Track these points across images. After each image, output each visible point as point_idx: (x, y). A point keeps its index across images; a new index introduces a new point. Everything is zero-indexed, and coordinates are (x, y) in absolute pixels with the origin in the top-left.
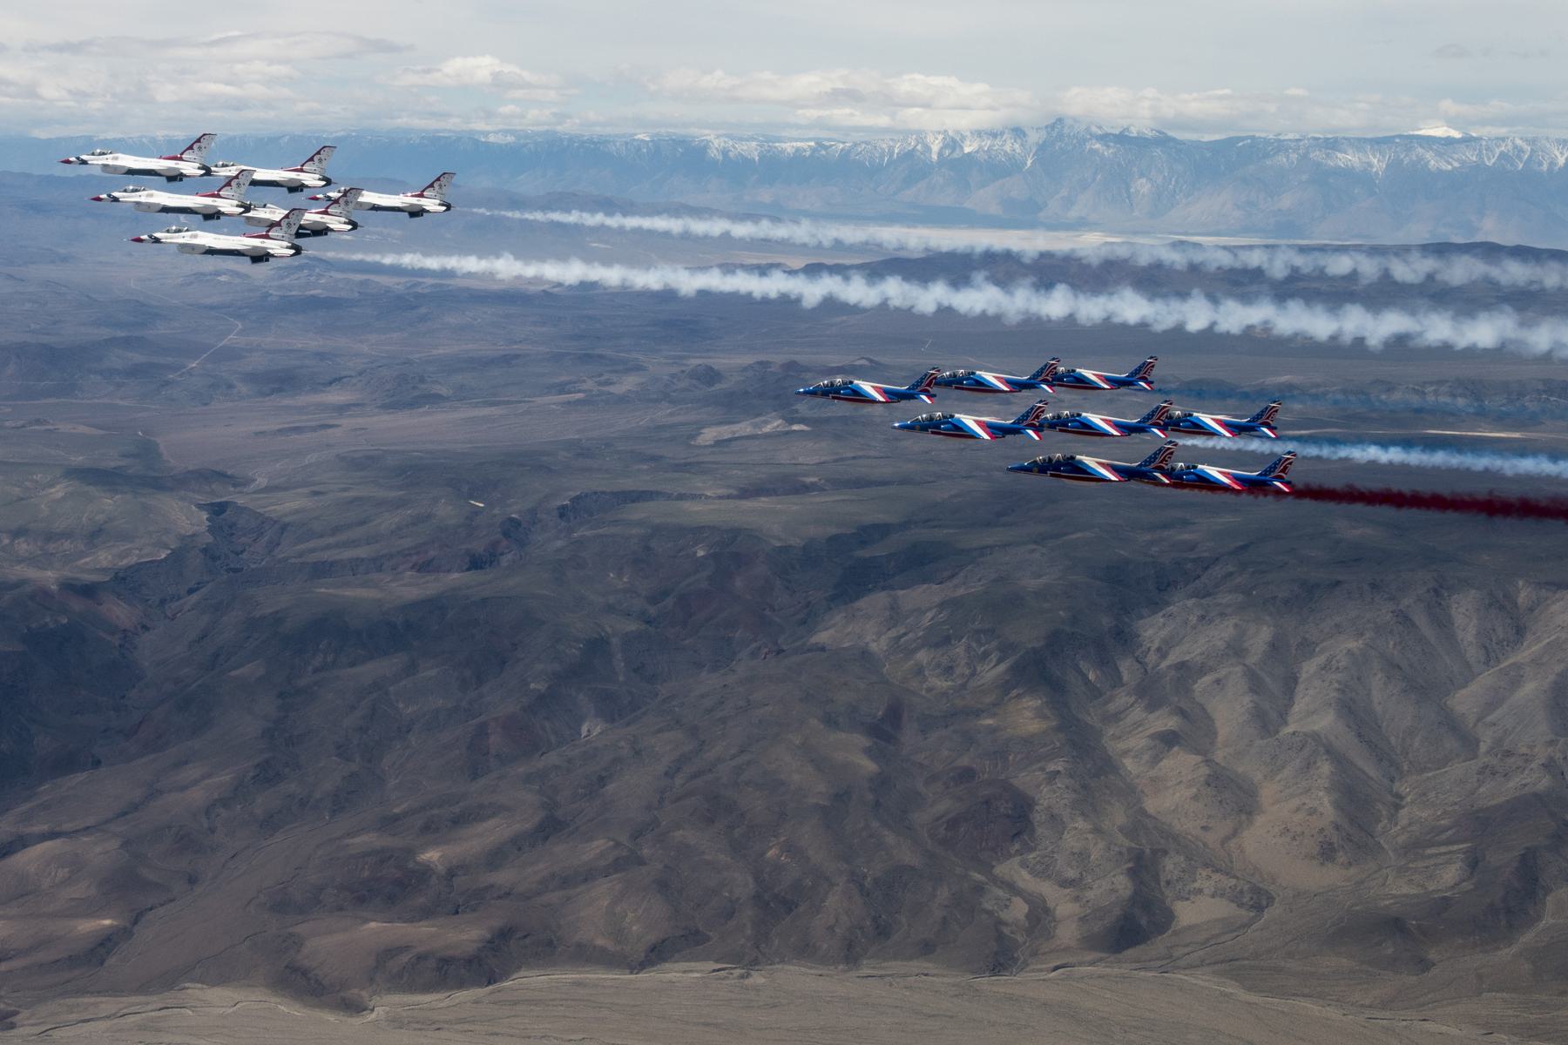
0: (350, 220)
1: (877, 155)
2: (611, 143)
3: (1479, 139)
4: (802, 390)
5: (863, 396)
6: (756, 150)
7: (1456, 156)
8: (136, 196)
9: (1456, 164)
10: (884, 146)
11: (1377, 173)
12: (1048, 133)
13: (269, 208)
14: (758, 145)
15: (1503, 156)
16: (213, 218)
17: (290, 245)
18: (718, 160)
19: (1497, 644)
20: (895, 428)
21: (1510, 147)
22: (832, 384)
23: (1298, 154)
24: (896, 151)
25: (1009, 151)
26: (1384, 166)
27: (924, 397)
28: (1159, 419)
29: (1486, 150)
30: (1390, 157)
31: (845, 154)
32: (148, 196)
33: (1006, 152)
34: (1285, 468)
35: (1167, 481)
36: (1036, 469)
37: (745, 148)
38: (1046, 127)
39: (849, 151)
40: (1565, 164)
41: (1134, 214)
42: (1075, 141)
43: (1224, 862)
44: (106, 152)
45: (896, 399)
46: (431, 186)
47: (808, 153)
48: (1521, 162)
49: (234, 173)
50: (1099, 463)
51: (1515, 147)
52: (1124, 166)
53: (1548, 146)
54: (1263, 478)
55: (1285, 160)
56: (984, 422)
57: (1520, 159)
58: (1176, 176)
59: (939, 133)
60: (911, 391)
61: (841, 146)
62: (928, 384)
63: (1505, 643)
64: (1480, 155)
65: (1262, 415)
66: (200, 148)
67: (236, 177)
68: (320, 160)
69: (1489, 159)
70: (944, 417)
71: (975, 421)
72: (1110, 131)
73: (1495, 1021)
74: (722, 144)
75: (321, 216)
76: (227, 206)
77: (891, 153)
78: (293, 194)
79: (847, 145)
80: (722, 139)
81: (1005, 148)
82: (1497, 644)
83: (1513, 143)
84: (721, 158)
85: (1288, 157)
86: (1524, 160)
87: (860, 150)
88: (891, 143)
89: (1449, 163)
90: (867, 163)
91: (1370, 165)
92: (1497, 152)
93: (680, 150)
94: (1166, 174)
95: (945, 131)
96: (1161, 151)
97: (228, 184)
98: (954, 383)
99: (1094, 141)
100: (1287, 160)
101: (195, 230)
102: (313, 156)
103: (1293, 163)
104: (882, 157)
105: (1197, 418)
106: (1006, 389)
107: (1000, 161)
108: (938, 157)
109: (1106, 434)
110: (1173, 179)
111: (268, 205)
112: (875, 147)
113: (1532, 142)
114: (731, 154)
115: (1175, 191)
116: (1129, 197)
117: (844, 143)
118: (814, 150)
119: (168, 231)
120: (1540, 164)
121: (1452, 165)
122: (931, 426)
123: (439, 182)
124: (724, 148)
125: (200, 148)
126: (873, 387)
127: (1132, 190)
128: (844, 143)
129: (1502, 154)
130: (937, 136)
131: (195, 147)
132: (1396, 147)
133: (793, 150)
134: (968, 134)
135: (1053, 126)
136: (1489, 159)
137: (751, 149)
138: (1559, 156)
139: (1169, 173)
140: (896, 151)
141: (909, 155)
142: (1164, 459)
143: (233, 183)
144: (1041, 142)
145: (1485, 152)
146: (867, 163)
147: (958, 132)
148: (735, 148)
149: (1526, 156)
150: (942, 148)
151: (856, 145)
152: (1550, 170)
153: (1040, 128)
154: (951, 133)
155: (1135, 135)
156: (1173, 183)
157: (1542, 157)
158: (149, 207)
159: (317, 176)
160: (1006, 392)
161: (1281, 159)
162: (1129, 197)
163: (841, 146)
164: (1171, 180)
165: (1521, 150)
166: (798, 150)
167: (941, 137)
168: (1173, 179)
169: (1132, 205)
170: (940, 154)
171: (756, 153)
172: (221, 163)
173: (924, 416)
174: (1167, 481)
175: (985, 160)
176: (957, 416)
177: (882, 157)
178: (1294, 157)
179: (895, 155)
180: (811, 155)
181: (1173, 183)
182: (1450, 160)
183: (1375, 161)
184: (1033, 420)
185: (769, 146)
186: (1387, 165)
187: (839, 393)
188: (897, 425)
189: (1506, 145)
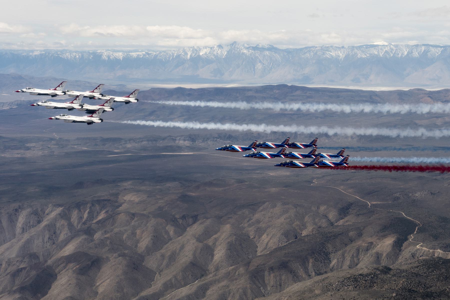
1: (168, 57)
2: (65, 54)
3: (377, 46)
4: (217, 149)
6: (122, 55)
7: (368, 52)
8: (46, 104)
9: (368, 55)
10: (171, 53)
11: (341, 59)
12: (231, 47)
14: (122, 54)
15: (386, 52)
16: (71, 110)
17: (99, 119)
18: (106, 60)
19: (29, 227)
20: (244, 157)
21: (389, 48)
22: (226, 147)
23: (314, 53)
24: (175, 55)
25: (216, 54)
26: (344, 57)
27: (253, 149)
28: (314, 153)
29: (381, 50)
30: (346, 53)
31: (156, 56)
32: (50, 104)
33: (214, 54)
35: (318, 166)
36: (282, 165)
37: (117, 55)
38: (231, 45)
39: (157, 56)
41: (255, 77)
43: (260, 244)
45: (245, 150)
46: (59, 86)
47: (142, 56)
48: (392, 53)
51: (391, 48)
52: (254, 59)
53: (402, 48)
55: (309, 55)
56: (269, 154)
57: (391, 52)
59: (191, 47)
60: (309, 155)
61: (155, 53)
62: (254, 146)
63: (32, 227)
64: (378, 52)
65: (285, 142)
69: (381, 53)
70: (258, 153)
71: (266, 153)
72: (252, 46)
74: (108, 54)
75: (71, 104)
76: (76, 106)
77: (173, 55)
79: (157, 53)
80: (108, 52)
81: (214, 53)
82: (29, 227)
83: (390, 47)
84: (107, 59)
85: (310, 54)
86: (393, 53)
87: (161, 55)
88: (173, 52)
89: (366, 55)
90: (164, 60)
91: (339, 56)
92: (384, 50)
93: (92, 56)
95: (194, 47)
96: (268, 53)
98: (260, 146)
99: (244, 50)
100: (310, 55)
103: (311, 56)
104: (169, 58)
105: (267, 144)
106: (274, 147)
107: (212, 58)
108: (190, 57)
109: (238, 151)
110: (272, 63)
112: (167, 53)
113: (396, 46)
114: (111, 58)
115: (272, 68)
116: (254, 71)
117: (156, 52)
119: (60, 116)
120: (398, 54)
121: (366, 56)
122: (254, 156)
123: (61, 85)
124: (109, 55)
128: (156, 52)
129: (386, 50)
130: (190, 49)
133: (137, 55)
134: (202, 48)
135: (233, 44)
136: (381, 53)
137: (120, 55)
138: (405, 50)
140: (175, 55)
141: (178, 56)
142: (317, 161)
144: (228, 50)
145: (380, 50)
146: (164, 60)
149: (394, 52)
151: (160, 53)
154: (195, 48)
155: (261, 47)
156: (271, 64)
157: (399, 52)
158: (50, 107)
160: (275, 148)
162: (254, 71)
163: (155, 53)
164: (270, 63)
165: (393, 50)
166: (138, 55)
167: (191, 49)
168: (272, 63)
169: (255, 73)
171: (121, 57)
172: (28, 88)
173: (252, 153)
174: (318, 166)
176: (261, 152)
177: (169, 58)
179: (175, 57)
180: (142, 58)
181: (271, 64)
182: (366, 54)
183: (341, 55)
184: (283, 152)
185: (127, 54)
187: (228, 149)
188: (244, 156)
189: (388, 48)
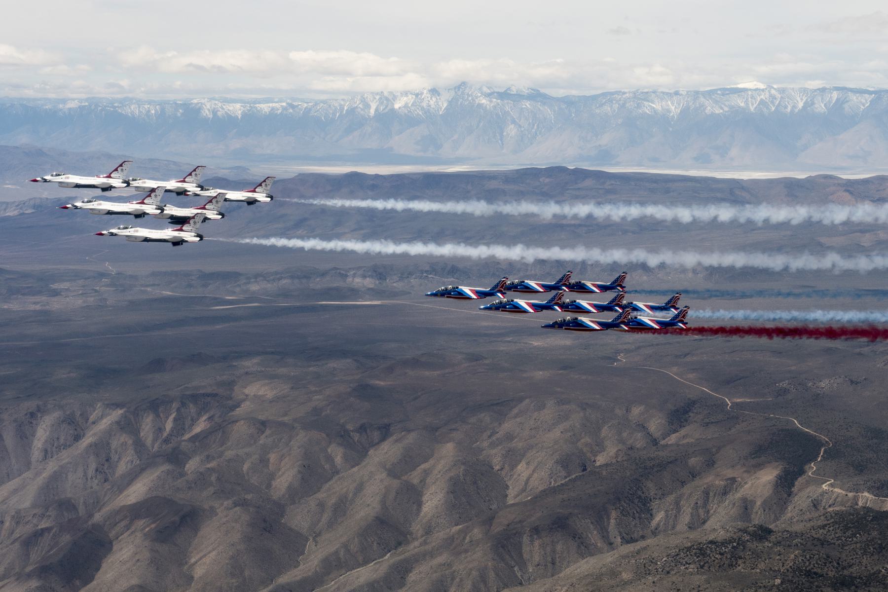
0: (220, 212)
3: (745, 90)
5: (583, 309)
7: (727, 103)
8: (90, 205)
9: (726, 109)
10: (337, 105)
11: (673, 116)
12: (456, 93)
13: (167, 207)
15: (762, 102)
16: (141, 217)
17: (196, 234)
18: (209, 118)
20: (481, 309)
21: (767, 95)
22: (446, 289)
23: (619, 104)
24: (346, 109)
25: (425, 107)
26: (679, 112)
27: (499, 294)
29: (751, 98)
30: (683, 105)
31: (308, 111)
32: (98, 204)
33: (423, 107)
34: (684, 315)
35: (627, 329)
36: (557, 326)
37: (231, 108)
38: (455, 88)
39: (310, 110)
40: (803, 107)
41: (503, 151)
42: (470, 98)
44: (60, 173)
45: (483, 296)
47: (279, 111)
48: (774, 106)
49: (215, 195)
50: (591, 321)
51: (771, 96)
52: (501, 116)
54: (549, 304)
55: (609, 109)
56: (531, 303)
57: (772, 102)
58: (538, 123)
59: (377, 94)
60: (610, 305)
61: (306, 105)
64: (746, 102)
66: (122, 170)
67: (216, 197)
68: (196, 175)
70: (508, 301)
71: (526, 303)
73: (829, 522)
74: (213, 106)
75: (140, 205)
76: (150, 209)
78: (249, 206)
80: (214, 102)
83: (770, 93)
84: (211, 116)
85: (611, 107)
87: (319, 108)
89: (722, 108)
90: (323, 118)
91: (669, 111)
93: (181, 111)
94: (531, 121)
95: (382, 92)
96: (529, 104)
97: (211, 201)
100: (611, 109)
101: (137, 227)
102: (191, 173)
103: (614, 111)
104: (334, 114)
108: (375, 112)
110: (536, 125)
111: (167, 205)
113: (782, 91)
114: (219, 114)
115: (536, 134)
116: (501, 140)
117: (308, 103)
118: (285, 109)
120: (786, 107)
121: (723, 110)
122: (501, 307)
125: (122, 170)
126: (587, 303)
127: (505, 134)
129: (762, 100)
130: (376, 96)
131: (119, 169)
132: (688, 97)
133: (270, 109)
134: (399, 94)
135: (459, 87)
136: (753, 104)
137: (237, 109)
139: (533, 120)
140: (346, 109)
141: (352, 111)
142: (625, 317)
143: (213, 201)
145: (750, 99)
146: (323, 118)
147: (391, 93)
148: (223, 109)
149: (778, 102)
150: (378, 105)
151: (316, 104)
152: (792, 111)
153: (451, 89)
154: (386, 94)
155: (515, 93)
156: (535, 127)
157: (788, 103)
158: (99, 212)
159: (195, 185)
161: (607, 108)
162: (501, 140)
163: (306, 105)
165: (775, 98)
166: (273, 109)
167: (378, 97)
168: (536, 125)
170: (376, 110)
171: (240, 112)
173: (497, 301)
175: (405, 114)
176: (515, 300)
177: (334, 114)
178: (616, 106)
179: (345, 112)
180: (281, 113)
181: (535, 127)
182: (723, 106)
183: (673, 108)
184: (558, 300)
185: (250, 107)
186: (681, 111)
187: (451, 294)
188: (482, 307)
189: (765, 94)
